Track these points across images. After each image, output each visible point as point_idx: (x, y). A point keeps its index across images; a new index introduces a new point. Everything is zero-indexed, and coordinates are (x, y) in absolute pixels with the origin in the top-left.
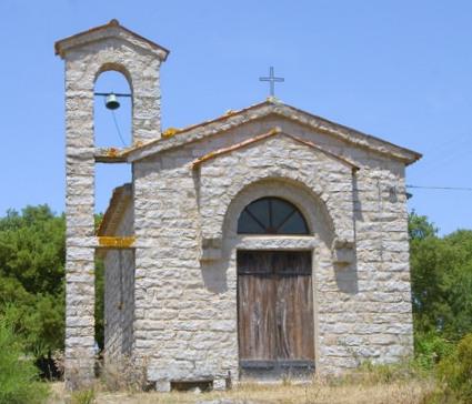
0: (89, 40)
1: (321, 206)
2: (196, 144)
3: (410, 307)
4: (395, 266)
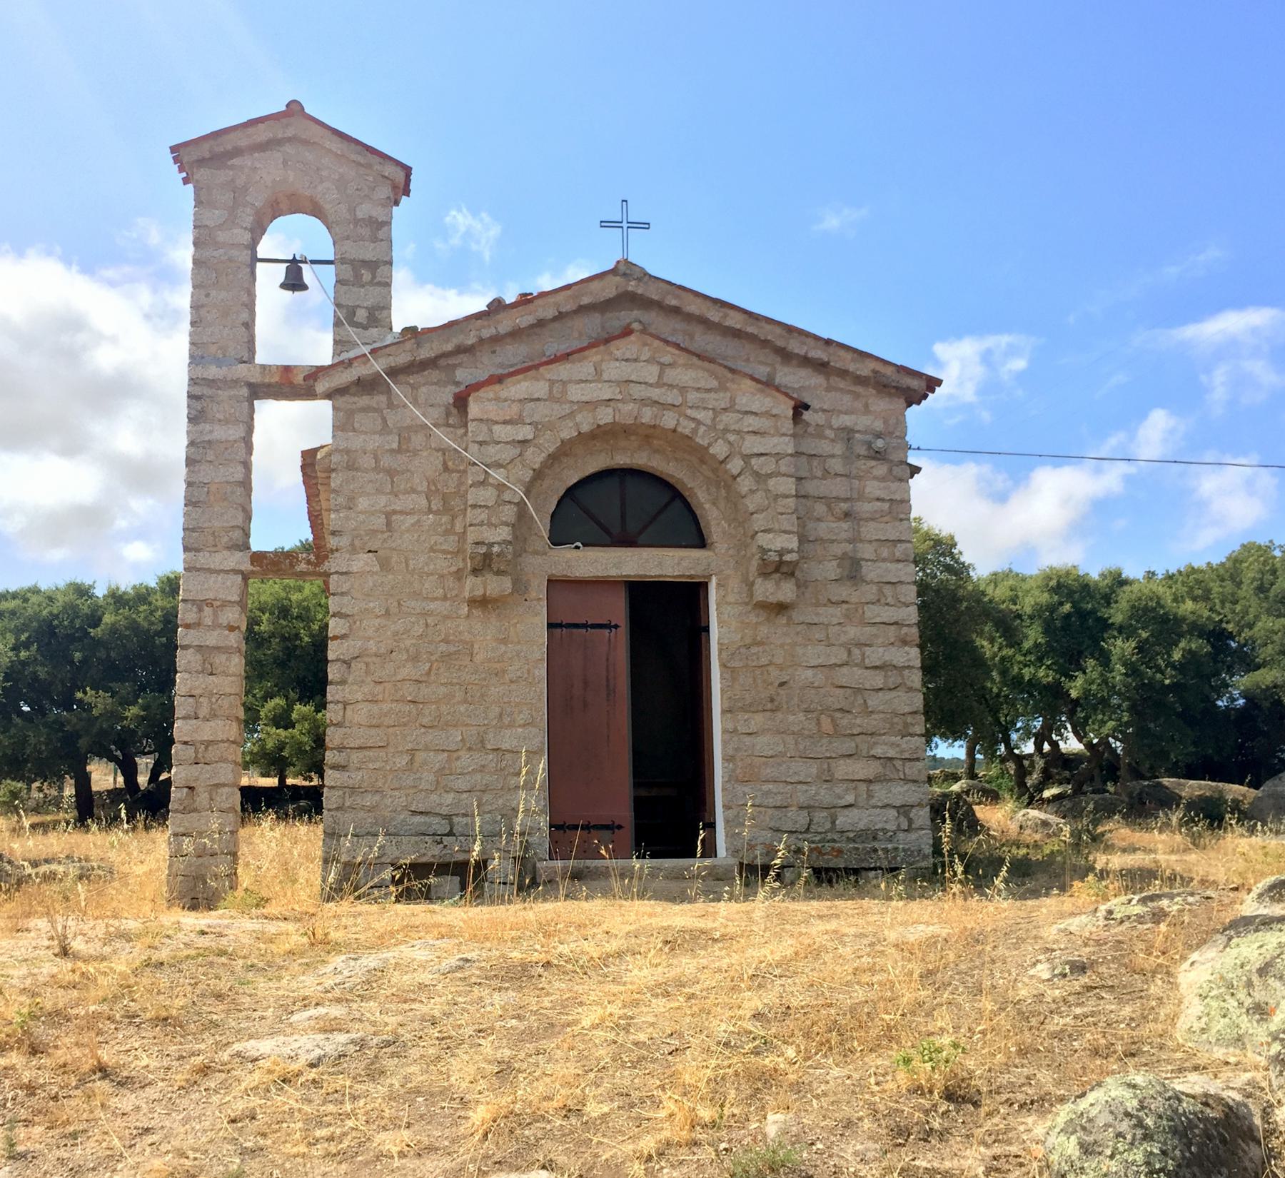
0: (243, 143)
1: (728, 487)
2: (463, 358)
3: (918, 701)
4: (887, 614)
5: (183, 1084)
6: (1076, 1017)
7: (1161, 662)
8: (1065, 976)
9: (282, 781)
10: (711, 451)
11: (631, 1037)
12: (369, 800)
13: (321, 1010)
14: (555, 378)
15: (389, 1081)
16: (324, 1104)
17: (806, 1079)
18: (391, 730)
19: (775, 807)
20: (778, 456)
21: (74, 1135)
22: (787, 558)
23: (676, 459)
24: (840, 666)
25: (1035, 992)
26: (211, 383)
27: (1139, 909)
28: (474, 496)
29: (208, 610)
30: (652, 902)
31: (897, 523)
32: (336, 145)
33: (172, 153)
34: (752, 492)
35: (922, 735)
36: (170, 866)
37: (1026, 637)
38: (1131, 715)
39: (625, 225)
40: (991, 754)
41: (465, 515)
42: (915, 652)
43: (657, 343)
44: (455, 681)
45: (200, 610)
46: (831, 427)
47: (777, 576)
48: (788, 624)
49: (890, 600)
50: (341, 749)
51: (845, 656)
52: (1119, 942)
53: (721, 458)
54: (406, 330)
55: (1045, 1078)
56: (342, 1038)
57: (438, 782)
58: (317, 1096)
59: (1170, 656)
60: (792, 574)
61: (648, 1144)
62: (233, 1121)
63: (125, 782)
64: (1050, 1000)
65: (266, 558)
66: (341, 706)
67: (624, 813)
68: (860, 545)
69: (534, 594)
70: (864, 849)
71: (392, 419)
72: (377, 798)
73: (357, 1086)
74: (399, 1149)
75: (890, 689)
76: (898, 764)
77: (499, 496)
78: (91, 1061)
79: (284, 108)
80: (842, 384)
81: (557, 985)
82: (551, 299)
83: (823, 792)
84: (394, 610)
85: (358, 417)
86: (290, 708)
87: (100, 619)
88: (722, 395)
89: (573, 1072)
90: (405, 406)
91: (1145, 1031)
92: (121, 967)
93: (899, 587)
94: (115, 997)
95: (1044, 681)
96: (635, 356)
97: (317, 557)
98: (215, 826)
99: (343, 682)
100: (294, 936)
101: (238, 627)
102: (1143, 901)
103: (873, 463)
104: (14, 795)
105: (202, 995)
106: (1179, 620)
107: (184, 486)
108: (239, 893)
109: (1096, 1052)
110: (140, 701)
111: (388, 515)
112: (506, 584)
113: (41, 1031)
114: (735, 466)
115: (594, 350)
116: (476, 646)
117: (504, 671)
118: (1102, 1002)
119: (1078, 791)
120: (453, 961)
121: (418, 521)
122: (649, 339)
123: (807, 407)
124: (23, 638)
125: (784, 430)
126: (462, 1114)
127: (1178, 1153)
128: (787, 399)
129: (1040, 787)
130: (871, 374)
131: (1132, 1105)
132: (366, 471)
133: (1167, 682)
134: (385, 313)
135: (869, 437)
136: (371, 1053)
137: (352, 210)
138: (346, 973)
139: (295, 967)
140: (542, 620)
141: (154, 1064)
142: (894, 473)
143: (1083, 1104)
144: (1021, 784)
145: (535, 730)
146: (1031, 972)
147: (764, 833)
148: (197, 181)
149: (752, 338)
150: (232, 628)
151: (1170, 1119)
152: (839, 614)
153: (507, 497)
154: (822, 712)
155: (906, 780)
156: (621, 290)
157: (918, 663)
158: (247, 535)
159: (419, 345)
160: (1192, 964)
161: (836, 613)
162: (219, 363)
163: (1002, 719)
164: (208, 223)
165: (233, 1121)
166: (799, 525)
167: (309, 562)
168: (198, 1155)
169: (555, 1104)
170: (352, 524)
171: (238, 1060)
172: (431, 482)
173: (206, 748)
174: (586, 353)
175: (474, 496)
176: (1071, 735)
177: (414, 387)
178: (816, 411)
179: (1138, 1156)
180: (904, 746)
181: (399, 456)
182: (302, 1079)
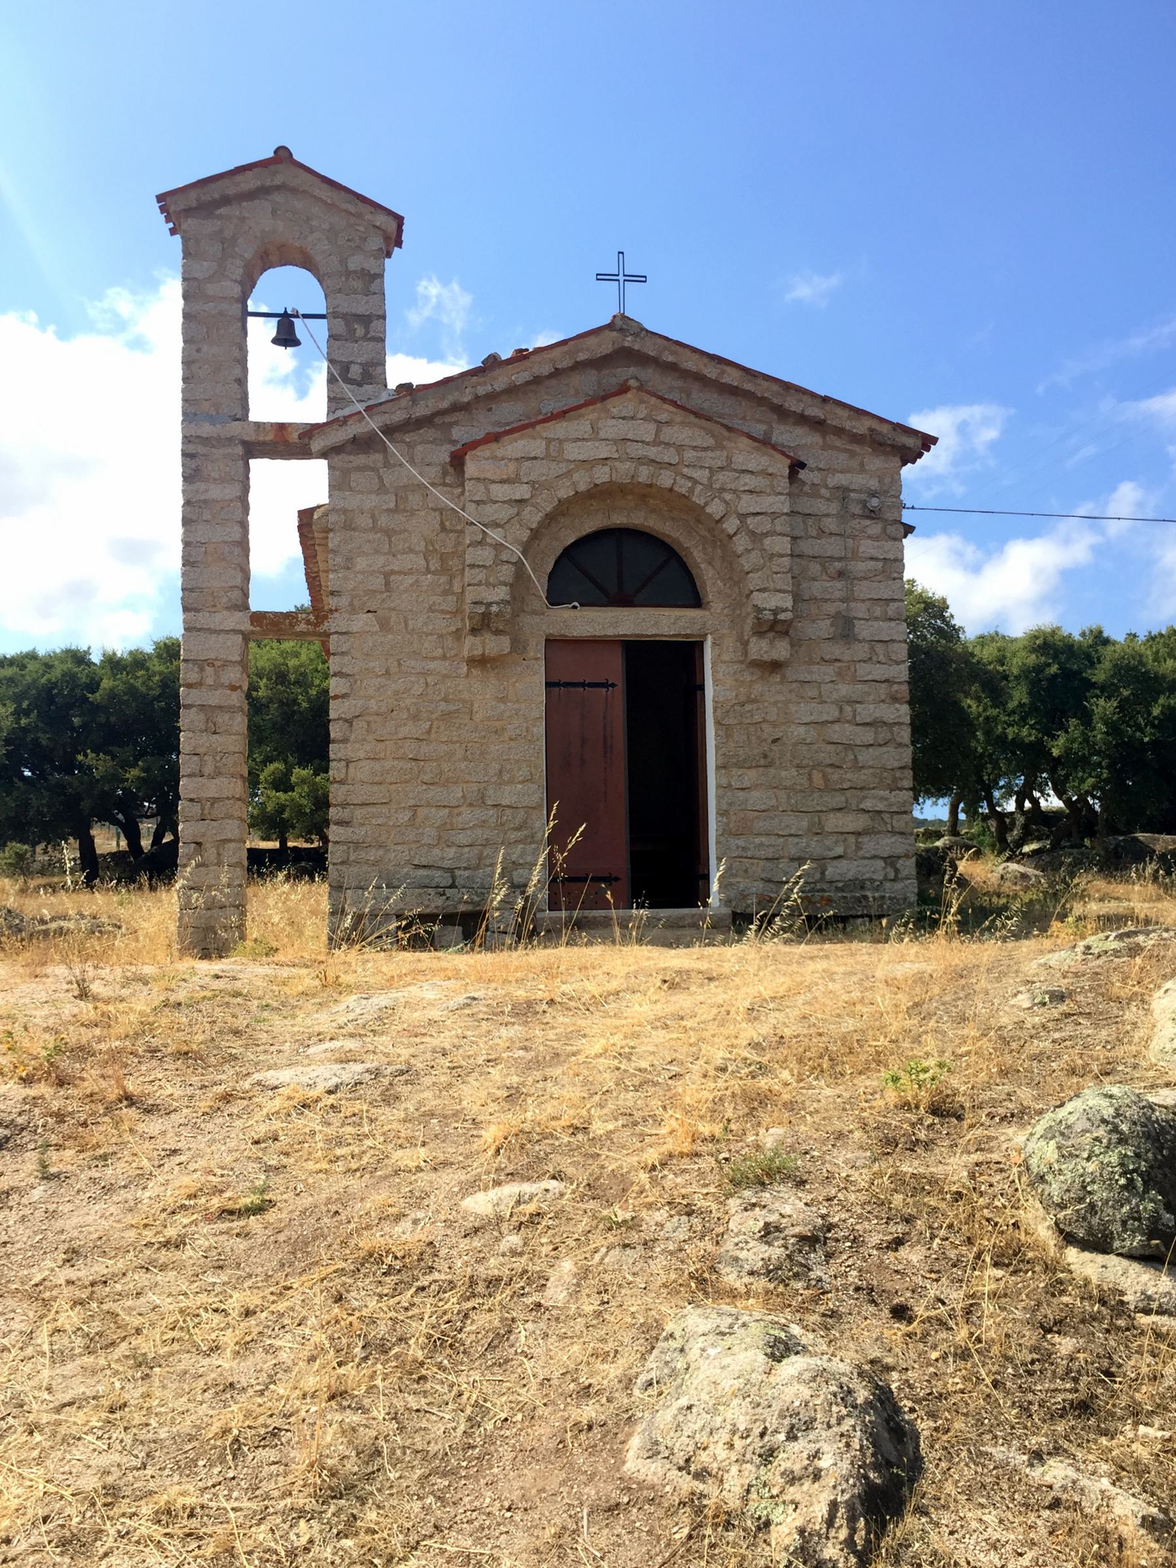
0: (231, 191)
3: (907, 755)
4: (879, 672)
5: (208, 1110)
6: (1054, 1041)
7: (1141, 720)
8: (1044, 1004)
9: (283, 843)
10: (708, 510)
11: (633, 1065)
12: (373, 855)
13: (336, 1044)
14: (552, 436)
15: (404, 1105)
16: (343, 1125)
17: (799, 1098)
18: (393, 787)
19: (767, 859)
20: (774, 515)
21: (104, 1157)
22: (782, 616)
23: (673, 519)
24: (832, 722)
25: (1016, 1020)
26: (205, 441)
27: (1116, 945)
28: (471, 556)
29: (209, 670)
30: (649, 947)
31: (890, 582)
32: (325, 193)
33: (159, 201)
34: (748, 551)
35: (911, 789)
36: (180, 919)
37: (1011, 697)
38: (1110, 772)
39: (621, 278)
40: (972, 812)
41: (463, 575)
42: (905, 709)
43: (653, 400)
44: (455, 739)
45: (202, 670)
46: (826, 487)
47: (771, 635)
48: (781, 682)
49: (881, 658)
50: (344, 805)
51: (837, 714)
52: (1097, 974)
53: (718, 517)
54: (401, 387)
55: (1025, 1095)
56: (358, 1068)
57: (440, 837)
58: (336, 1120)
59: (1149, 713)
60: (786, 633)
61: (652, 1156)
62: (257, 1142)
63: (129, 845)
64: (1029, 1026)
65: (265, 618)
66: (343, 763)
67: (621, 864)
68: (852, 605)
69: (532, 654)
70: (852, 897)
71: (389, 478)
72: (381, 852)
73: (374, 1110)
74: (416, 1164)
75: (880, 745)
76: (886, 817)
77: (496, 556)
78: (116, 1091)
79: (271, 155)
80: (838, 443)
81: (561, 1019)
82: (547, 355)
83: (813, 844)
84: (394, 668)
85: (353, 476)
86: (289, 772)
87: (98, 685)
88: (718, 453)
89: (578, 1095)
90: (401, 465)
91: (1119, 1052)
92: (140, 1007)
93: (890, 646)
94: (136, 1034)
95: (1027, 740)
96: (631, 414)
97: (317, 617)
98: (224, 880)
99: (345, 741)
100: (307, 980)
101: (240, 687)
102: (1120, 937)
103: (868, 522)
104: (20, 857)
105: (221, 1032)
106: (1158, 678)
107: (181, 546)
108: (249, 943)
109: (1073, 1072)
110: (140, 763)
111: (387, 575)
112: (504, 643)
113: (66, 1064)
114: (731, 525)
115: (591, 407)
116: (476, 705)
117: (503, 729)
118: (1079, 1027)
119: (1055, 846)
120: (461, 999)
121: (417, 581)
122: (646, 397)
123: (802, 465)
124: (25, 705)
125: (779, 489)
126: (475, 1133)
127: (1150, 1155)
128: (783, 458)
129: (1020, 843)
130: (867, 432)
131: (1108, 1112)
132: (365, 531)
133: (1146, 740)
134: (379, 369)
135: (863, 496)
136: (386, 1081)
137: (343, 262)
138: (358, 1011)
139: (309, 1005)
140: (541, 678)
141: (178, 1093)
142: (888, 531)
143: (1062, 1113)
144: (1002, 839)
145: (534, 786)
146: (1012, 1002)
147: (756, 884)
148: (185, 231)
149: (748, 395)
150: (234, 688)
151: (1144, 1125)
152: (832, 672)
153: (504, 557)
154: (814, 767)
155: (893, 832)
156: (616, 346)
157: (907, 720)
158: (246, 595)
159: (414, 402)
160: (1166, 991)
161: (830, 671)
162: (212, 420)
163: (986, 778)
164: (197, 275)
165: (257, 1142)
166: (793, 584)
167: (308, 622)
168: (226, 1172)
169: (563, 1123)
170: (351, 585)
171: (259, 1088)
172: (429, 542)
173: (212, 805)
174: (583, 411)
175: (471, 556)
176: (1051, 792)
177: (411, 446)
178: (812, 470)
179: (1113, 1157)
180: (893, 800)
181: (396, 516)
182: (320, 1105)
